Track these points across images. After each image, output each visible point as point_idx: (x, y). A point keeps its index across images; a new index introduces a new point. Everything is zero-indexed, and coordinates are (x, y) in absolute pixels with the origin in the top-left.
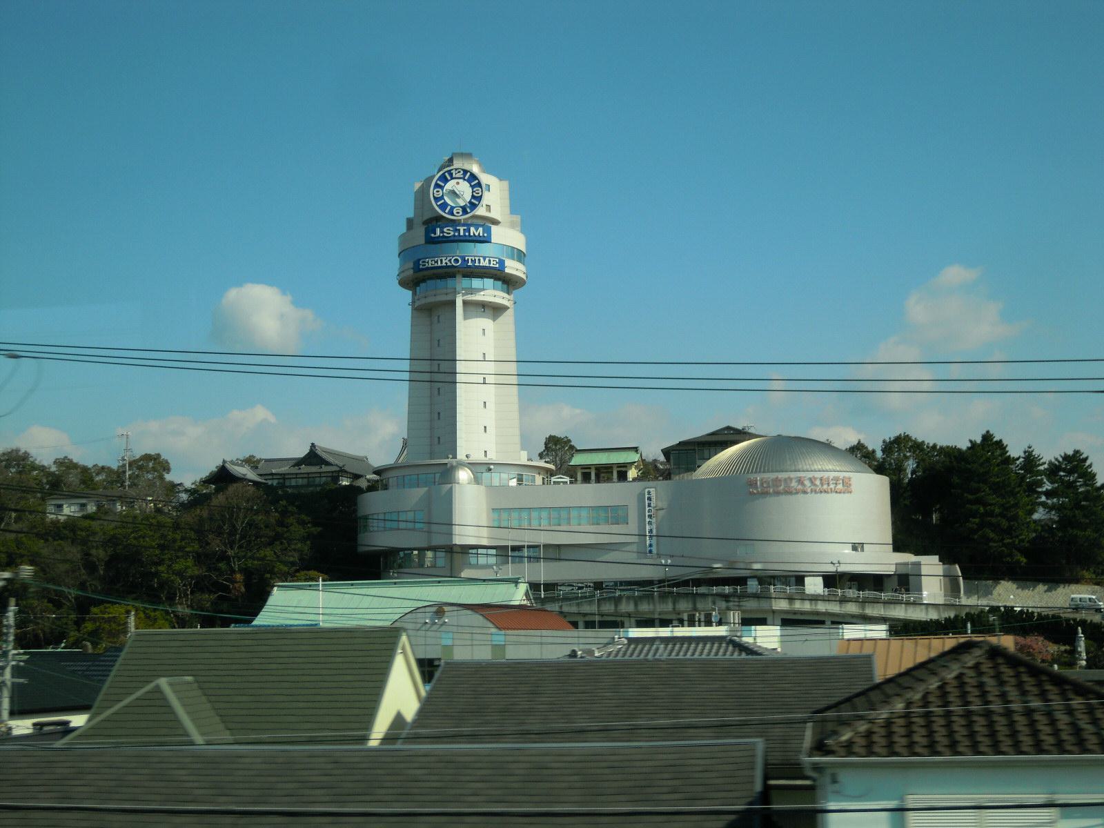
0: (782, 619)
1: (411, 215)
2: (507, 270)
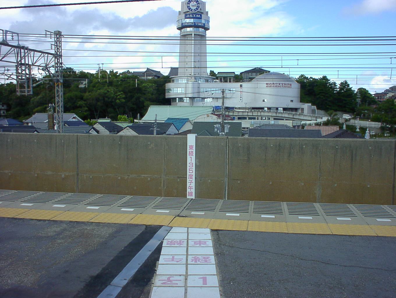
1: (180, 10)
2: (206, 26)
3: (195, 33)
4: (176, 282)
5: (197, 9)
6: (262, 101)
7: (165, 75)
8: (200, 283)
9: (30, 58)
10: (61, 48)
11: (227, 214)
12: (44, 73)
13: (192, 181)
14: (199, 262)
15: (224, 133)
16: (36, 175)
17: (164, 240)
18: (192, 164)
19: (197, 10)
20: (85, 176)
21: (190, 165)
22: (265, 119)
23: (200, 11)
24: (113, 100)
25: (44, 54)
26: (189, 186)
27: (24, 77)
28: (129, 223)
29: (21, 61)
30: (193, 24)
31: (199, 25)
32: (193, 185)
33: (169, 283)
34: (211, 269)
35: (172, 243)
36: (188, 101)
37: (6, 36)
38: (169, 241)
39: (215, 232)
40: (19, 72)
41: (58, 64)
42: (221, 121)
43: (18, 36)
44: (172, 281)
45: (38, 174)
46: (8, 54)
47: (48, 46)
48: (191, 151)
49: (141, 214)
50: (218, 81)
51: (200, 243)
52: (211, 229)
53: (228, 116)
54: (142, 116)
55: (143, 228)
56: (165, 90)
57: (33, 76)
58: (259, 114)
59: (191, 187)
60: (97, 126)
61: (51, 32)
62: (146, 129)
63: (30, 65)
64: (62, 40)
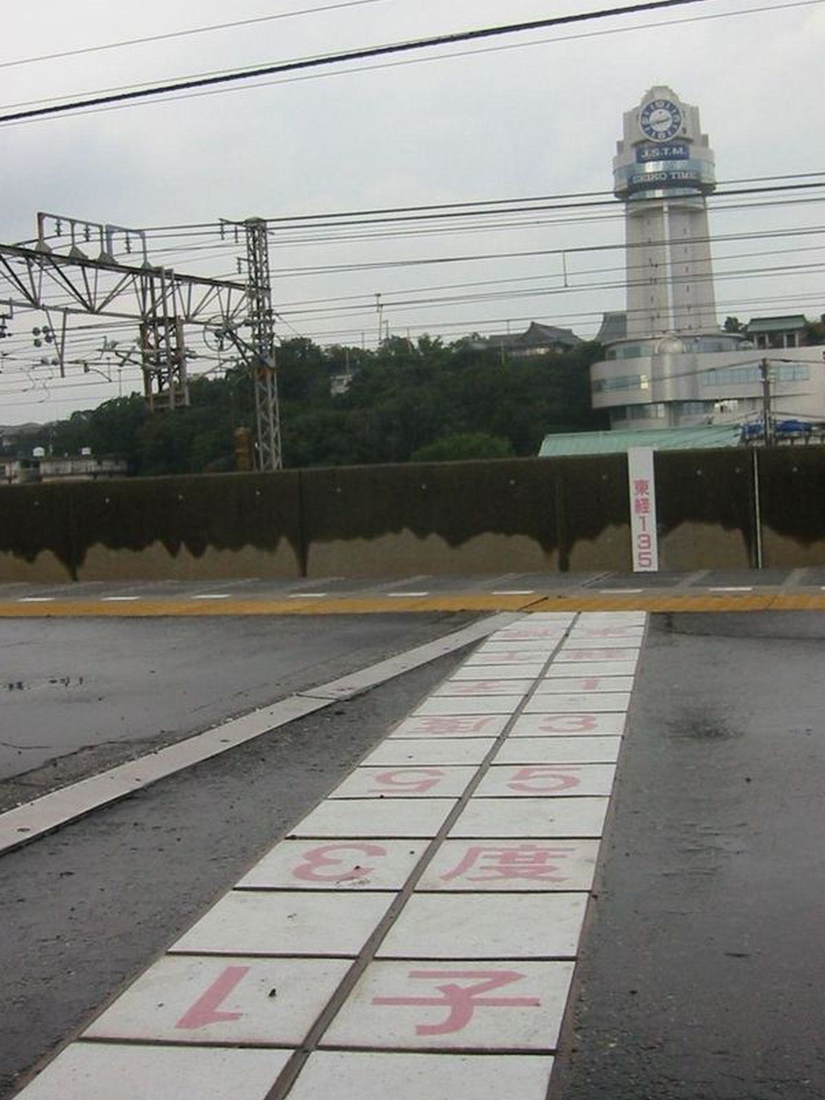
0: (655, 453)
1: (621, 138)
4: (428, 989)
5: (673, 130)
7: (588, 339)
10: (267, 267)
18: (646, 538)
19: (672, 134)
23: (683, 136)
25: (220, 288)
27: (165, 358)
29: (153, 310)
31: (683, 177)
36: (663, 412)
37: (109, 240)
40: (149, 344)
43: (143, 237)
46: (119, 289)
47: (227, 260)
48: (642, 500)
50: (750, 344)
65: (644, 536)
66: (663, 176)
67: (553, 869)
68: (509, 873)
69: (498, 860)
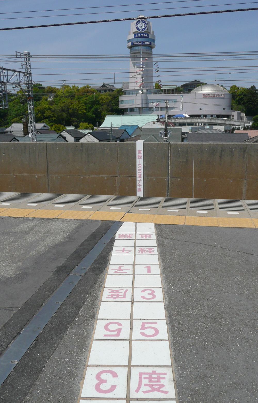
3: (143, 51)
4: (124, 271)
6: (199, 109)
8: (145, 271)
9: (4, 76)
11: (168, 210)
12: (18, 89)
13: (140, 179)
14: (145, 253)
15: (167, 138)
16: (15, 176)
17: (117, 234)
19: (144, 30)
20: (54, 176)
21: (139, 166)
22: (201, 125)
24: (76, 111)
26: (139, 184)
28: (88, 219)
30: (141, 43)
32: (142, 182)
33: (120, 271)
34: (154, 259)
35: (123, 236)
38: (121, 235)
39: (157, 226)
41: (29, 81)
42: (165, 127)
44: (123, 270)
45: (16, 176)
48: (140, 155)
49: (98, 211)
51: (146, 236)
52: (156, 224)
53: (171, 123)
54: (100, 124)
55: (100, 223)
56: (118, 101)
57: (8, 92)
58: (196, 120)
59: (140, 184)
60: (64, 134)
61: (21, 53)
62: (103, 136)
63: (4, 82)
64: (30, 59)
65: (140, 165)
66: (141, 43)
67: (110, 292)
68: (117, 291)
69: (120, 295)
